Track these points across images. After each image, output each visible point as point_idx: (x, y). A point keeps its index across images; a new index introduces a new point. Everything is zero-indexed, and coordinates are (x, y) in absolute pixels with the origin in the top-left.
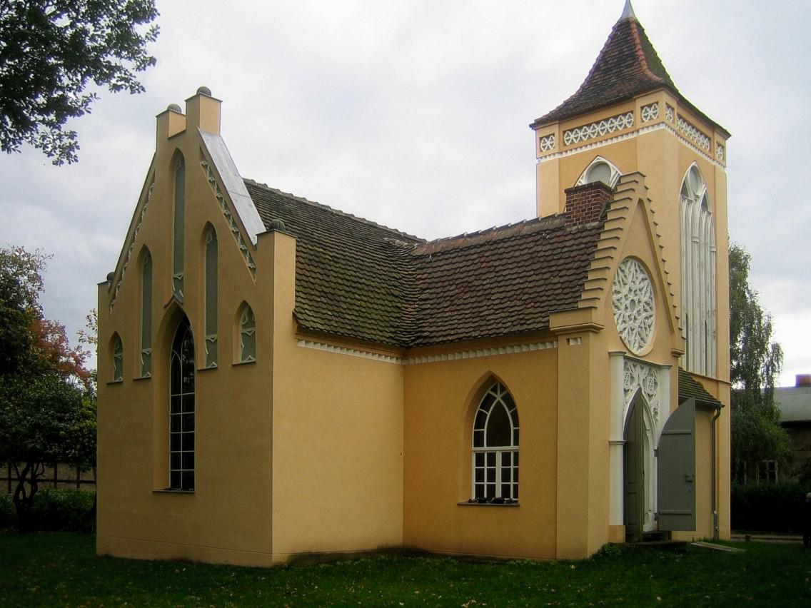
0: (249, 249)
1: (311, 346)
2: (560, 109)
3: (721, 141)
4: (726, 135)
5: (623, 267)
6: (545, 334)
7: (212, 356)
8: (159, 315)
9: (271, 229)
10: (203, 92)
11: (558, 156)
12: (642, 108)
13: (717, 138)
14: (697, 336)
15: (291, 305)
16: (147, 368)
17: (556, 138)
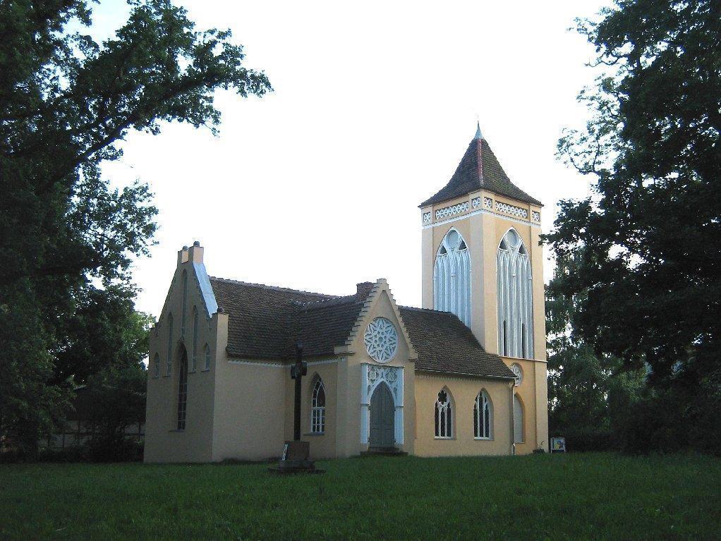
0: (209, 320)
1: (235, 362)
2: (432, 198)
3: (536, 209)
4: (540, 205)
5: (374, 323)
6: (333, 355)
7: (195, 367)
8: (175, 346)
9: (219, 310)
10: (196, 244)
11: (431, 226)
12: (473, 200)
13: (532, 208)
14: (515, 336)
15: (225, 344)
16: (169, 370)
17: (431, 214)
